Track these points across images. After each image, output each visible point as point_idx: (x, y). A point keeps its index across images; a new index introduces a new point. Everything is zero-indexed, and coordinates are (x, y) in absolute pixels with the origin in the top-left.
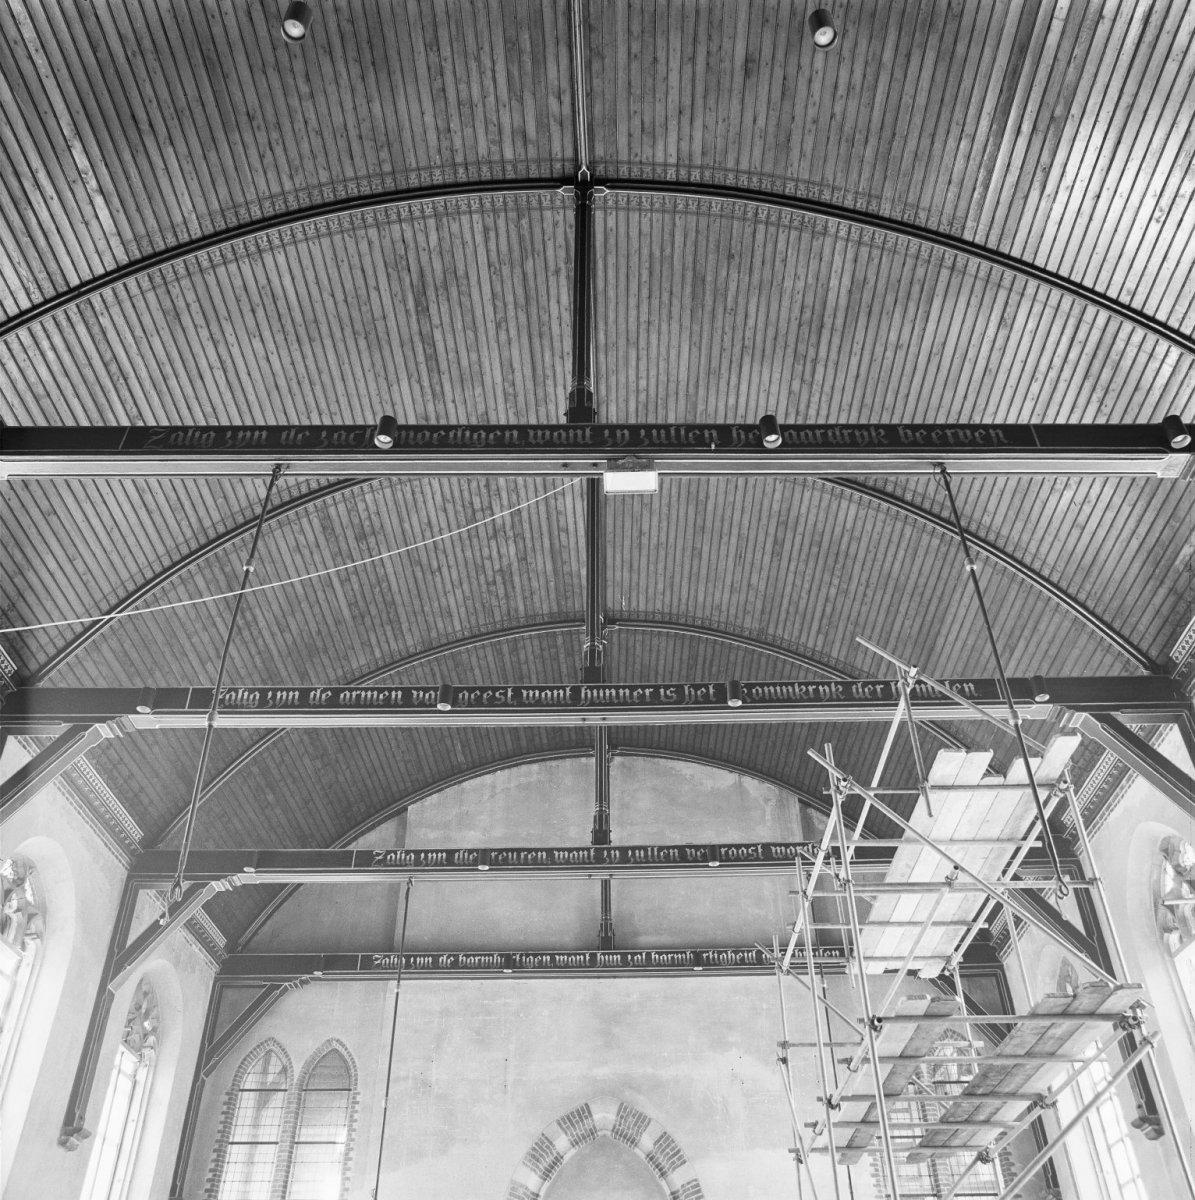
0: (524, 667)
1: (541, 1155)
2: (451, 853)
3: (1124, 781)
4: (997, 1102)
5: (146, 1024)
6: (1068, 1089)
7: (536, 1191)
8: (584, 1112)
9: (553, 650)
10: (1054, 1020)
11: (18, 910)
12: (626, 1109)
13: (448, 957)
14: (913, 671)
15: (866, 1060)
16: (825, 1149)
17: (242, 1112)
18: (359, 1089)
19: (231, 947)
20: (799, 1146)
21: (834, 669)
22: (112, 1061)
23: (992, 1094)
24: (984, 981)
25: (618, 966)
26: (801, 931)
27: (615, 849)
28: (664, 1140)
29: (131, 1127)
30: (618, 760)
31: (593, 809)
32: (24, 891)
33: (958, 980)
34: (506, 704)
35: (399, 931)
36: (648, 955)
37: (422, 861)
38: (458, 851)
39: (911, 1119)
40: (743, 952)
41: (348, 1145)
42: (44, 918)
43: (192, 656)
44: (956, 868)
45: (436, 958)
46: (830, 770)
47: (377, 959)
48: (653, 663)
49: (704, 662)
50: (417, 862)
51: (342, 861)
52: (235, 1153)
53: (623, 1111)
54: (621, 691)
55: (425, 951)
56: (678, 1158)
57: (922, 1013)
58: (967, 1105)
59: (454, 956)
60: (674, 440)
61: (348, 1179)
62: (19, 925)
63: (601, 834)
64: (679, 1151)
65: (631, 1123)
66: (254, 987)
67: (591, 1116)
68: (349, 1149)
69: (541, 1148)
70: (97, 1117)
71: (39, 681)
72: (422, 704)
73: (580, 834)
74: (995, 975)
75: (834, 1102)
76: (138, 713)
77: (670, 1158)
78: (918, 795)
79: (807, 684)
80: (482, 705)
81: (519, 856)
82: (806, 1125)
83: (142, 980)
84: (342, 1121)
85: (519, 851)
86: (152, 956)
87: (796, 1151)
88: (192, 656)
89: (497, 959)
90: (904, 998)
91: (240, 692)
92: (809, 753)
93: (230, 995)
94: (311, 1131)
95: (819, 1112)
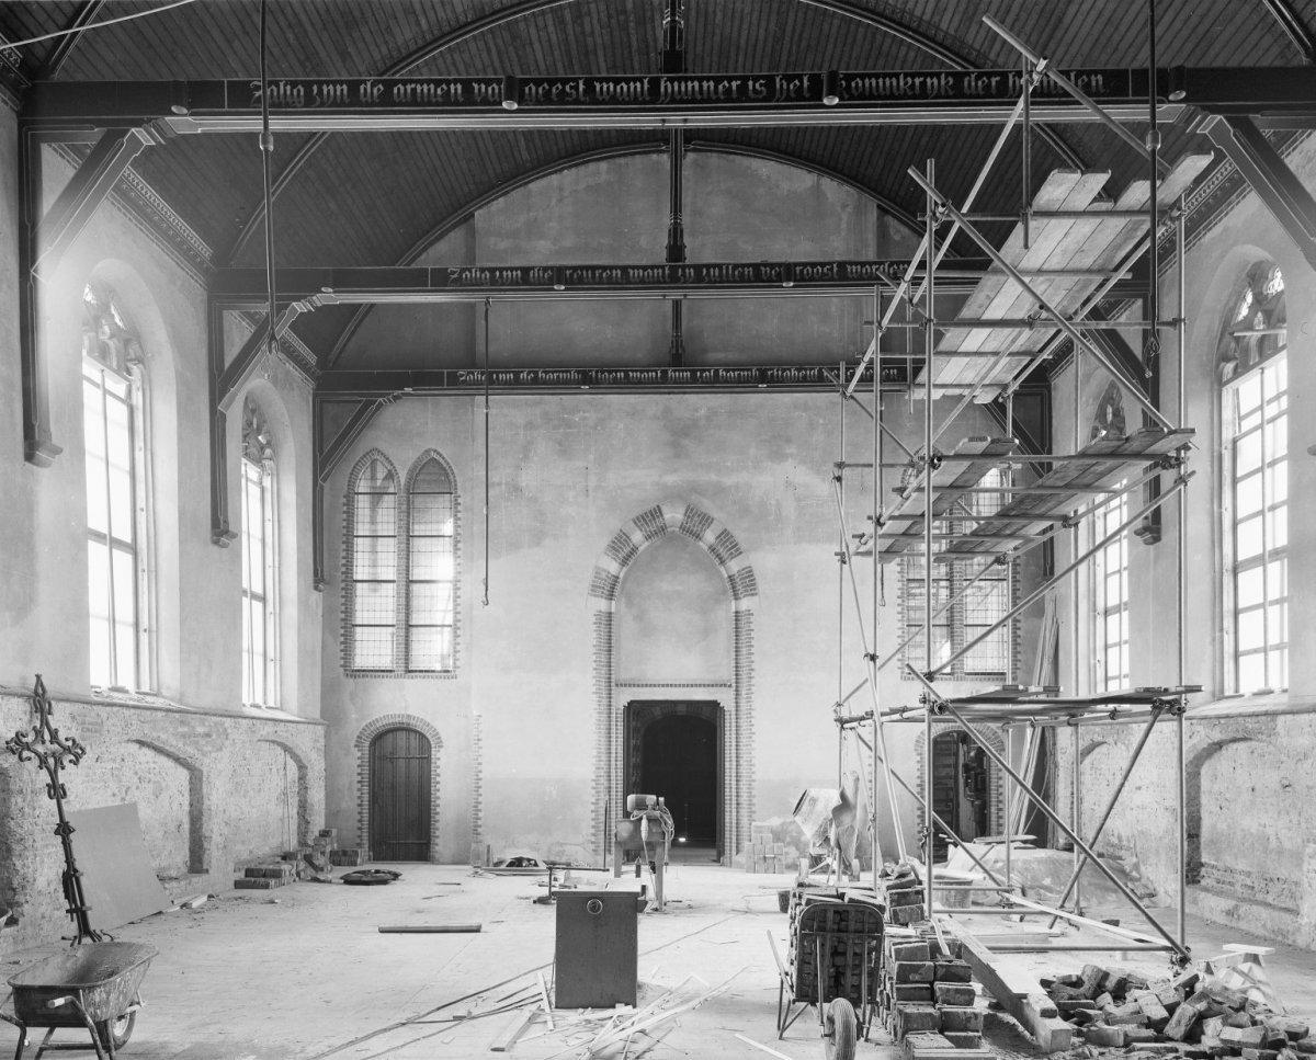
0: (589, 39)
1: (621, 547)
2: (526, 270)
3: (1233, 197)
4: (1024, 522)
5: (260, 438)
8: (656, 513)
9: (622, 18)
11: (111, 337)
14: (1042, 64)
16: (868, 553)
19: (321, 364)
20: (844, 550)
21: (940, 45)
23: (1024, 515)
25: (687, 383)
27: (689, 267)
28: (725, 536)
30: (691, 156)
31: (667, 221)
33: (1010, 406)
34: (577, 101)
35: (480, 348)
36: (717, 371)
37: (496, 279)
38: (533, 268)
40: (806, 370)
43: (215, 33)
44: (1041, 307)
45: (517, 374)
46: (929, 192)
48: (735, 35)
49: (793, 34)
50: (493, 281)
51: (417, 281)
52: (361, 545)
53: (690, 512)
54: (705, 84)
55: (505, 366)
56: (735, 550)
62: (118, 352)
63: (676, 250)
64: (736, 545)
65: (696, 521)
67: (662, 515)
71: (54, 69)
72: (485, 101)
73: (652, 248)
75: (882, 520)
76: (175, 114)
78: (1016, 223)
79: (913, 76)
80: (551, 102)
81: (593, 274)
82: (853, 536)
83: (246, 398)
84: (447, 504)
85: (593, 268)
88: (215, 33)
89: (574, 375)
90: (966, 440)
91: (282, 85)
92: (910, 171)
94: (422, 527)
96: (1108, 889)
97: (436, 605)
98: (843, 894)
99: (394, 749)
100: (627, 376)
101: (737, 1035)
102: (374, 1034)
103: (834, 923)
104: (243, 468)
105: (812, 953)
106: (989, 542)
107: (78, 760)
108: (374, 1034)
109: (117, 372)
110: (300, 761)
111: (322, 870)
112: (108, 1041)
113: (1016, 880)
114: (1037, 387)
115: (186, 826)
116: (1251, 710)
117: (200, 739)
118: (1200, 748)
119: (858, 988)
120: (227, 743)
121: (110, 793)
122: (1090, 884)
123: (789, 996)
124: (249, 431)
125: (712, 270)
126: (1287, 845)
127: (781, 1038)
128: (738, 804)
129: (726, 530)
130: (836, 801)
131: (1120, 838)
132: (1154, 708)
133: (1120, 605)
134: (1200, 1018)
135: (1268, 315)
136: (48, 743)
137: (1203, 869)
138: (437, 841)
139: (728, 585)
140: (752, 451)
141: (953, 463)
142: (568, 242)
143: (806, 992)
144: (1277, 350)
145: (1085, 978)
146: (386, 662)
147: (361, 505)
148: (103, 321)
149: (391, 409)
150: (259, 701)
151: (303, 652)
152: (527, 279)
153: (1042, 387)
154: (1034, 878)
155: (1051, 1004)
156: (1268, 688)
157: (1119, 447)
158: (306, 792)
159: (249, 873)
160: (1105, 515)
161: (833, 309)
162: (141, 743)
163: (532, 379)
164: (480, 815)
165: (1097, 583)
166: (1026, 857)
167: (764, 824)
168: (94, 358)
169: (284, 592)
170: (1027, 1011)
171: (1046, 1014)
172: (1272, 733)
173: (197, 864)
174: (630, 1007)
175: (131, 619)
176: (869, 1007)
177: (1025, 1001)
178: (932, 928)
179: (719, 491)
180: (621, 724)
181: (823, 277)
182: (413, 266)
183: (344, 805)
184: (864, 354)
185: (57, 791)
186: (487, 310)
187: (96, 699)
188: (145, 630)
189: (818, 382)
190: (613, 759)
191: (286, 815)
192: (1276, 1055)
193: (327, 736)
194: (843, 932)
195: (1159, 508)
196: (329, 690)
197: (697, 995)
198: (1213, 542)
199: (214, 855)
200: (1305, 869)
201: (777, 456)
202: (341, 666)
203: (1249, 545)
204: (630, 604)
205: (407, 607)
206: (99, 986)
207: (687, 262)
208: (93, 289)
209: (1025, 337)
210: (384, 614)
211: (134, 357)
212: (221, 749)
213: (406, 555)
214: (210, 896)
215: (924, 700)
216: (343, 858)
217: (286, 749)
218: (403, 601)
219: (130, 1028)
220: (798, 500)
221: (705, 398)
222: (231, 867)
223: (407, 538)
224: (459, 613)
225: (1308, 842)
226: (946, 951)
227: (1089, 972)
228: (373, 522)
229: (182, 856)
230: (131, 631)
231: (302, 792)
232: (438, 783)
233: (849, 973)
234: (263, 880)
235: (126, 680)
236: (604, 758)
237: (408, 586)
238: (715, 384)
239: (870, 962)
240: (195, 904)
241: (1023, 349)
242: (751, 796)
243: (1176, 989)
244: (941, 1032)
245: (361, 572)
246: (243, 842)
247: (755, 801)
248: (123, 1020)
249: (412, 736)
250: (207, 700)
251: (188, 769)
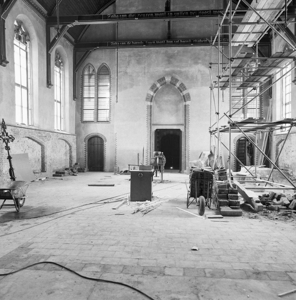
1: (153, 87)
2: (128, 15)
4: (260, 77)
5: (60, 60)
6: (280, 72)
7: (152, 95)
12: (173, 78)
13: (129, 42)
15: (228, 68)
16: (217, 87)
17: (85, 80)
18: (111, 74)
19: (76, 41)
22: (54, 69)
23: (259, 75)
24: (265, 47)
26: (218, 35)
27: (171, 12)
28: (182, 85)
29: (62, 83)
32: (22, 29)
35: (116, 36)
37: (120, 17)
38: (130, 14)
39: (241, 80)
40: (204, 40)
41: (110, 86)
42: (29, 36)
45: (126, 43)
47: (112, 43)
50: (119, 18)
51: (100, 18)
52: (86, 88)
53: (173, 78)
56: (185, 88)
58: (252, 78)
59: (131, 42)
60: (180, 15)
61: (111, 93)
62: (23, 38)
64: (185, 87)
65: (174, 81)
66: (83, 51)
68: (110, 87)
69: (153, 86)
70: (54, 82)
73: (162, 8)
74: (269, 45)
75: (220, 77)
77: (183, 89)
81: (146, 15)
82: (214, 82)
83: (56, 50)
85: (145, 13)
86: (57, 45)
87: (210, 87)
89: (141, 43)
91: (114, 15)
93: (78, 53)
94: (102, 83)
95: (217, 79)
96: (283, 178)
97: (104, 104)
98: (203, 170)
99: (94, 142)
100: (156, 42)
101: (176, 207)
102: (83, 205)
103: (200, 177)
104: (55, 68)
105: (195, 185)
106: (251, 83)
107: (13, 141)
108: (83, 205)
109: (23, 43)
110: (70, 145)
111: (75, 173)
112: (18, 204)
113: (259, 175)
114: (267, 43)
115: (41, 160)
117: (43, 137)
119: (206, 194)
120: (51, 139)
121: (21, 150)
122: (279, 177)
123: (189, 196)
124: (57, 59)
125: (177, 13)
127: (187, 208)
128: (185, 157)
129: (182, 83)
130: (209, 153)
131: (288, 165)
132: (291, 124)
133: (289, 102)
136: (5, 136)
138: (105, 166)
139: (183, 98)
140: (189, 62)
141: (238, 60)
142: (140, 8)
143: (192, 194)
145: (270, 195)
146: (92, 119)
147: (85, 78)
148: (20, 30)
149: (93, 52)
150: (59, 129)
151: (70, 117)
152: (128, 17)
153: (269, 43)
157: (281, 55)
158: (71, 153)
159: (57, 172)
160: (286, 78)
161: (211, 23)
162: (29, 138)
163: (130, 44)
164: (117, 159)
166: (262, 170)
167: (192, 162)
168: (17, 39)
169: (65, 101)
170: (252, 201)
171: (257, 202)
173: (43, 170)
174: (150, 201)
175: (26, 106)
176: (209, 199)
177: (252, 199)
178: (228, 181)
179: (180, 73)
180: (154, 135)
181: (207, 14)
182: (100, 14)
183: (81, 157)
184: (216, 33)
185: (8, 148)
186: (118, 25)
187: (17, 126)
188: (30, 109)
189: (207, 43)
190: (152, 145)
191: (66, 159)
193: (77, 138)
194: (203, 179)
196: (77, 126)
197: (167, 199)
199: (47, 167)
201: (196, 63)
202: (80, 120)
204: (156, 103)
205: (97, 104)
206: (16, 189)
207: (171, 11)
208: (17, 22)
209: (258, 28)
210: (91, 106)
211: (27, 39)
212: (49, 140)
213: (97, 91)
214: (46, 178)
215: (229, 123)
216: (81, 170)
217: (66, 142)
218: (96, 103)
219: (24, 202)
220: (202, 75)
221: (177, 48)
222: (52, 171)
223: (97, 87)
224: (111, 106)
226: (232, 186)
228: (89, 82)
229: (39, 167)
230: (26, 109)
231: (70, 153)
232: (106, 151)
233: (204, 190)
234: (60, 174)
235: (25, 122)
236: (149, 144)
237: (98, 99)
238: (179, 44)
239: (210, 187)
240: (43, 179)
241: (259, 31)
242: (188, 155)
243: (293, 197)
244: (229, 206)
245: (85, 95)
246: (55, 165)
247: (190, 156)
248: (22, 200)
249: (99, 138)
250: (46, 128)
251: (41, 145)
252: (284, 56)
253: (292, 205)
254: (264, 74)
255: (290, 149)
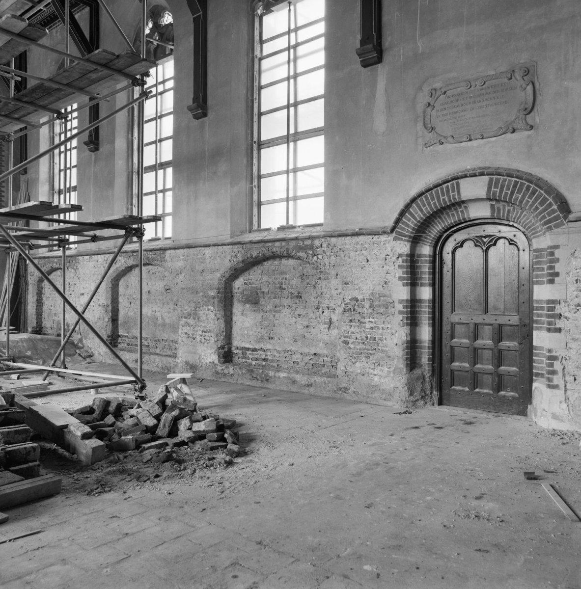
4: (31, 108)
10: (99, 68)
23: (31, 103)
57: (17, 32)
90: (9, 15)
116: (152, 247)
118: (121, 269)
126: (167, 321)
134: (176, 421)
135: (161, 35)
137: (120, 339)
144: (165, 55)
145: (95, 407)
154: (20, 352)
155: (87, 429)
156: (156, 237)
165: (55, 173)
170: (69, 437)
171: (86, 436)
172: (163, 260)
192: (223, 435)
195: (97, 128)
198: (128, 156)
200: (180, 333)
203: (149, 159)
225: (182, 317)
227: (97, 403)
244: (7, 469)
252: (114, 67)
253: (164, 425)
254: (46, 102)
255: (72, 289)
